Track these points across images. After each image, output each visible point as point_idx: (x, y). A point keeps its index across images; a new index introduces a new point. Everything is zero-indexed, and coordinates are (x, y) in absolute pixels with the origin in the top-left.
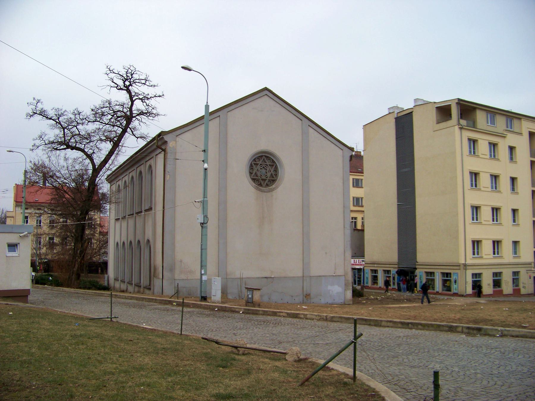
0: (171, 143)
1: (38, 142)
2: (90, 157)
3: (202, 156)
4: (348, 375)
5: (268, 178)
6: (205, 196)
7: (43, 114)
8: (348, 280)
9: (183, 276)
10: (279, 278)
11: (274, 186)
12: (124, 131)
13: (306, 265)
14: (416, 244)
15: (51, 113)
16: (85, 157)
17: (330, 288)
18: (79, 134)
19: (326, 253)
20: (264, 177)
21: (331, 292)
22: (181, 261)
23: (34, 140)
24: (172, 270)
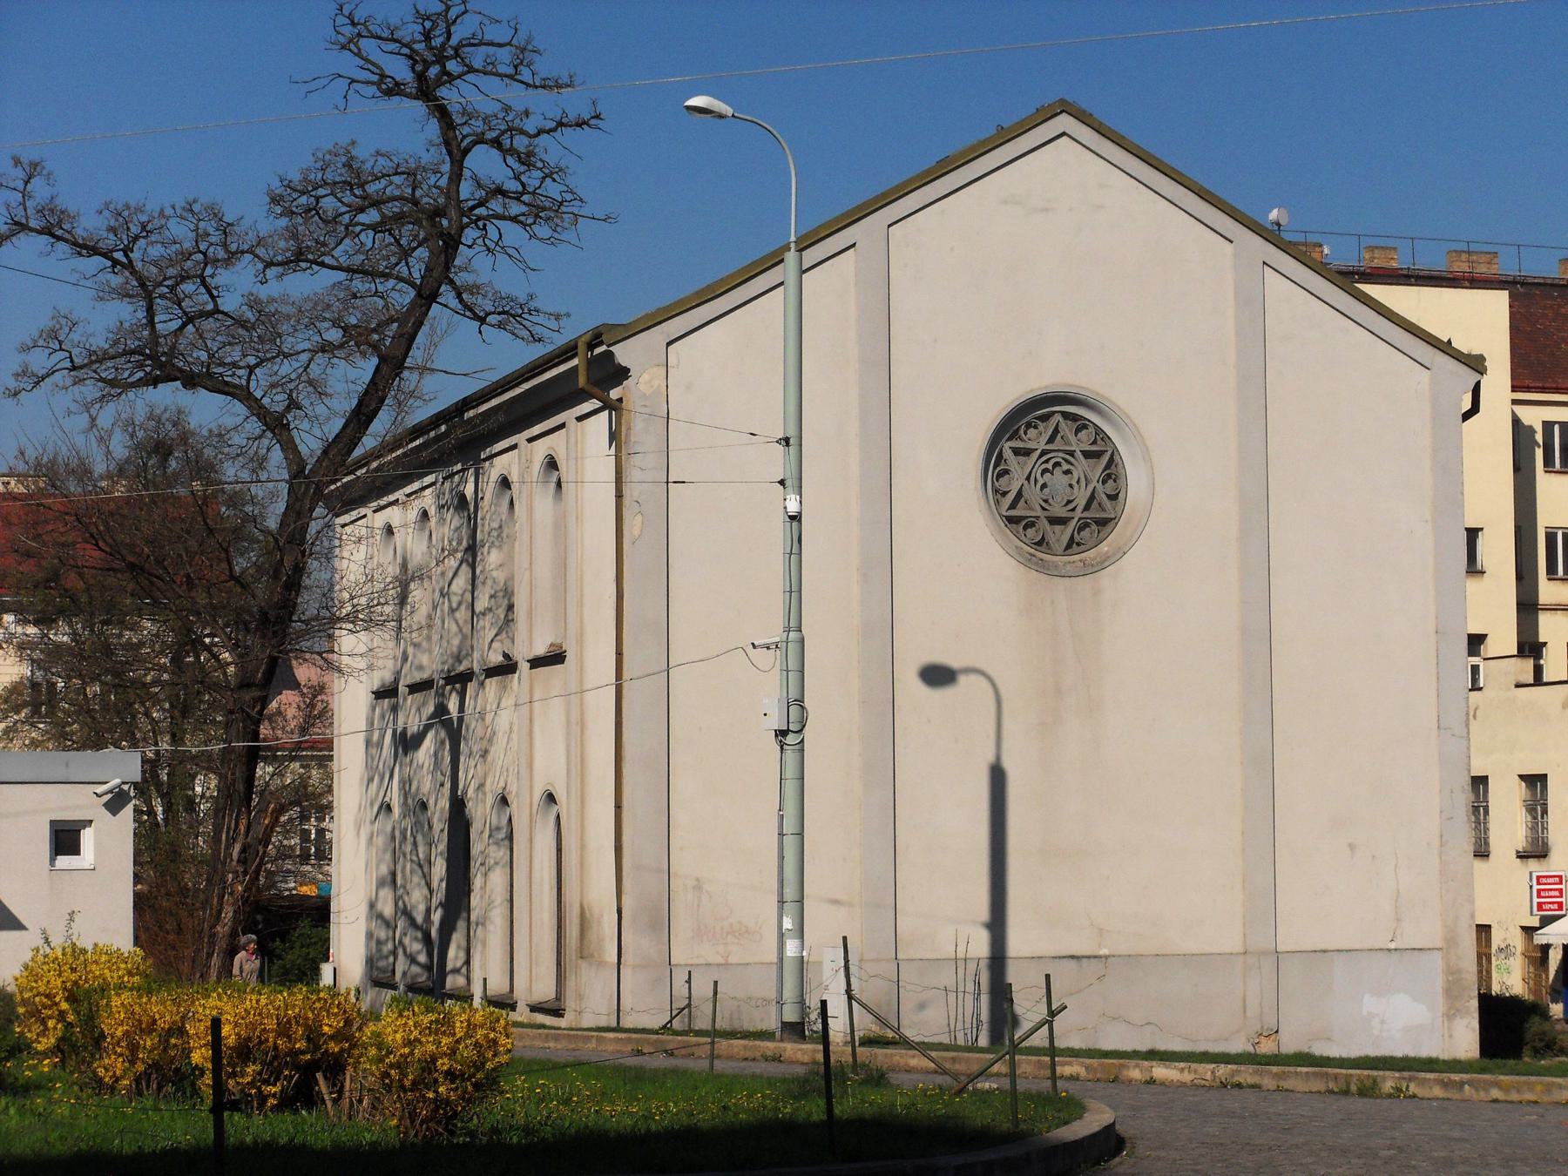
0: (646, 377)
1: (39, 361)
2: (277, 425)
3: (776, 462)
4: (1039, 1095)
5: (1078, 513)
6: (794, 624)
7: (54, 227)
8: (1459, 971)
9: (709, 953)
10: (1132, 959)
11: (1104, 547)
12: (427, 297)
13: (1263, 898)
14: (328, 949)
15: (90, 224)
16: (254, 426)
17: (1369, 1004)
18: (217, 311)
19: (1352, 847)
20: (1058, 511)
21: (1376, 1023)
22: (698, 887)
23: (25, 349)
24: (662, 922)
